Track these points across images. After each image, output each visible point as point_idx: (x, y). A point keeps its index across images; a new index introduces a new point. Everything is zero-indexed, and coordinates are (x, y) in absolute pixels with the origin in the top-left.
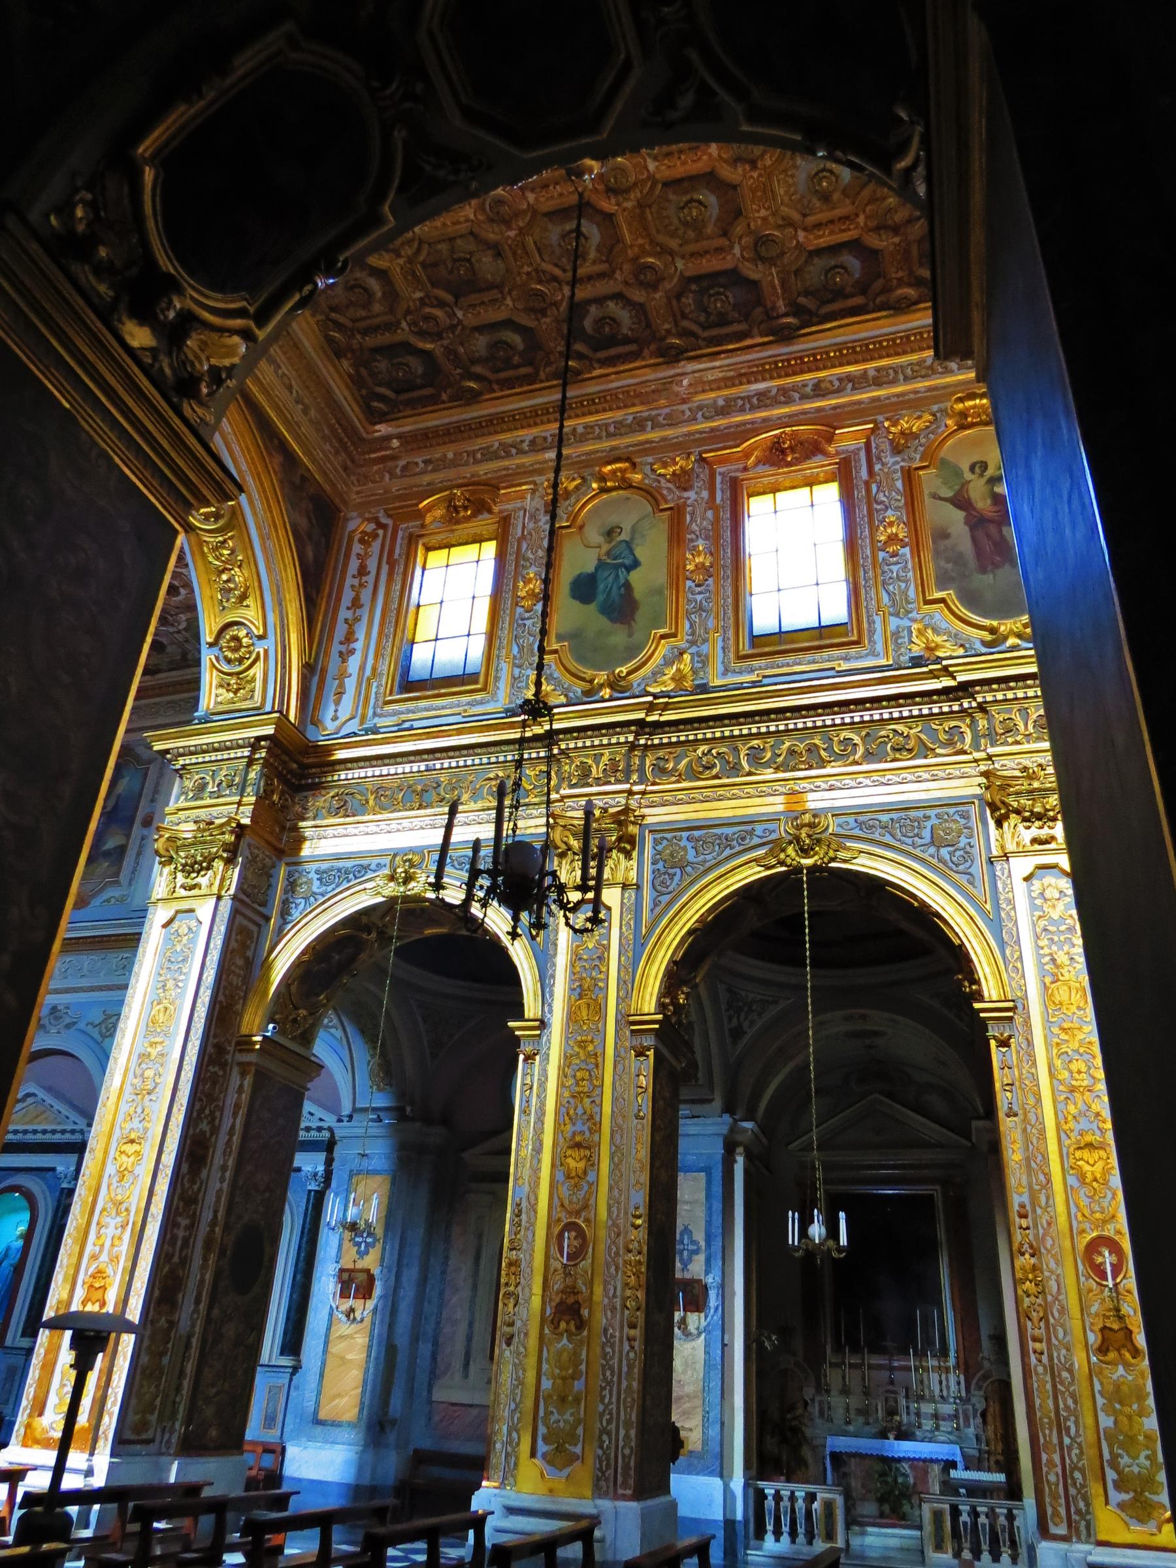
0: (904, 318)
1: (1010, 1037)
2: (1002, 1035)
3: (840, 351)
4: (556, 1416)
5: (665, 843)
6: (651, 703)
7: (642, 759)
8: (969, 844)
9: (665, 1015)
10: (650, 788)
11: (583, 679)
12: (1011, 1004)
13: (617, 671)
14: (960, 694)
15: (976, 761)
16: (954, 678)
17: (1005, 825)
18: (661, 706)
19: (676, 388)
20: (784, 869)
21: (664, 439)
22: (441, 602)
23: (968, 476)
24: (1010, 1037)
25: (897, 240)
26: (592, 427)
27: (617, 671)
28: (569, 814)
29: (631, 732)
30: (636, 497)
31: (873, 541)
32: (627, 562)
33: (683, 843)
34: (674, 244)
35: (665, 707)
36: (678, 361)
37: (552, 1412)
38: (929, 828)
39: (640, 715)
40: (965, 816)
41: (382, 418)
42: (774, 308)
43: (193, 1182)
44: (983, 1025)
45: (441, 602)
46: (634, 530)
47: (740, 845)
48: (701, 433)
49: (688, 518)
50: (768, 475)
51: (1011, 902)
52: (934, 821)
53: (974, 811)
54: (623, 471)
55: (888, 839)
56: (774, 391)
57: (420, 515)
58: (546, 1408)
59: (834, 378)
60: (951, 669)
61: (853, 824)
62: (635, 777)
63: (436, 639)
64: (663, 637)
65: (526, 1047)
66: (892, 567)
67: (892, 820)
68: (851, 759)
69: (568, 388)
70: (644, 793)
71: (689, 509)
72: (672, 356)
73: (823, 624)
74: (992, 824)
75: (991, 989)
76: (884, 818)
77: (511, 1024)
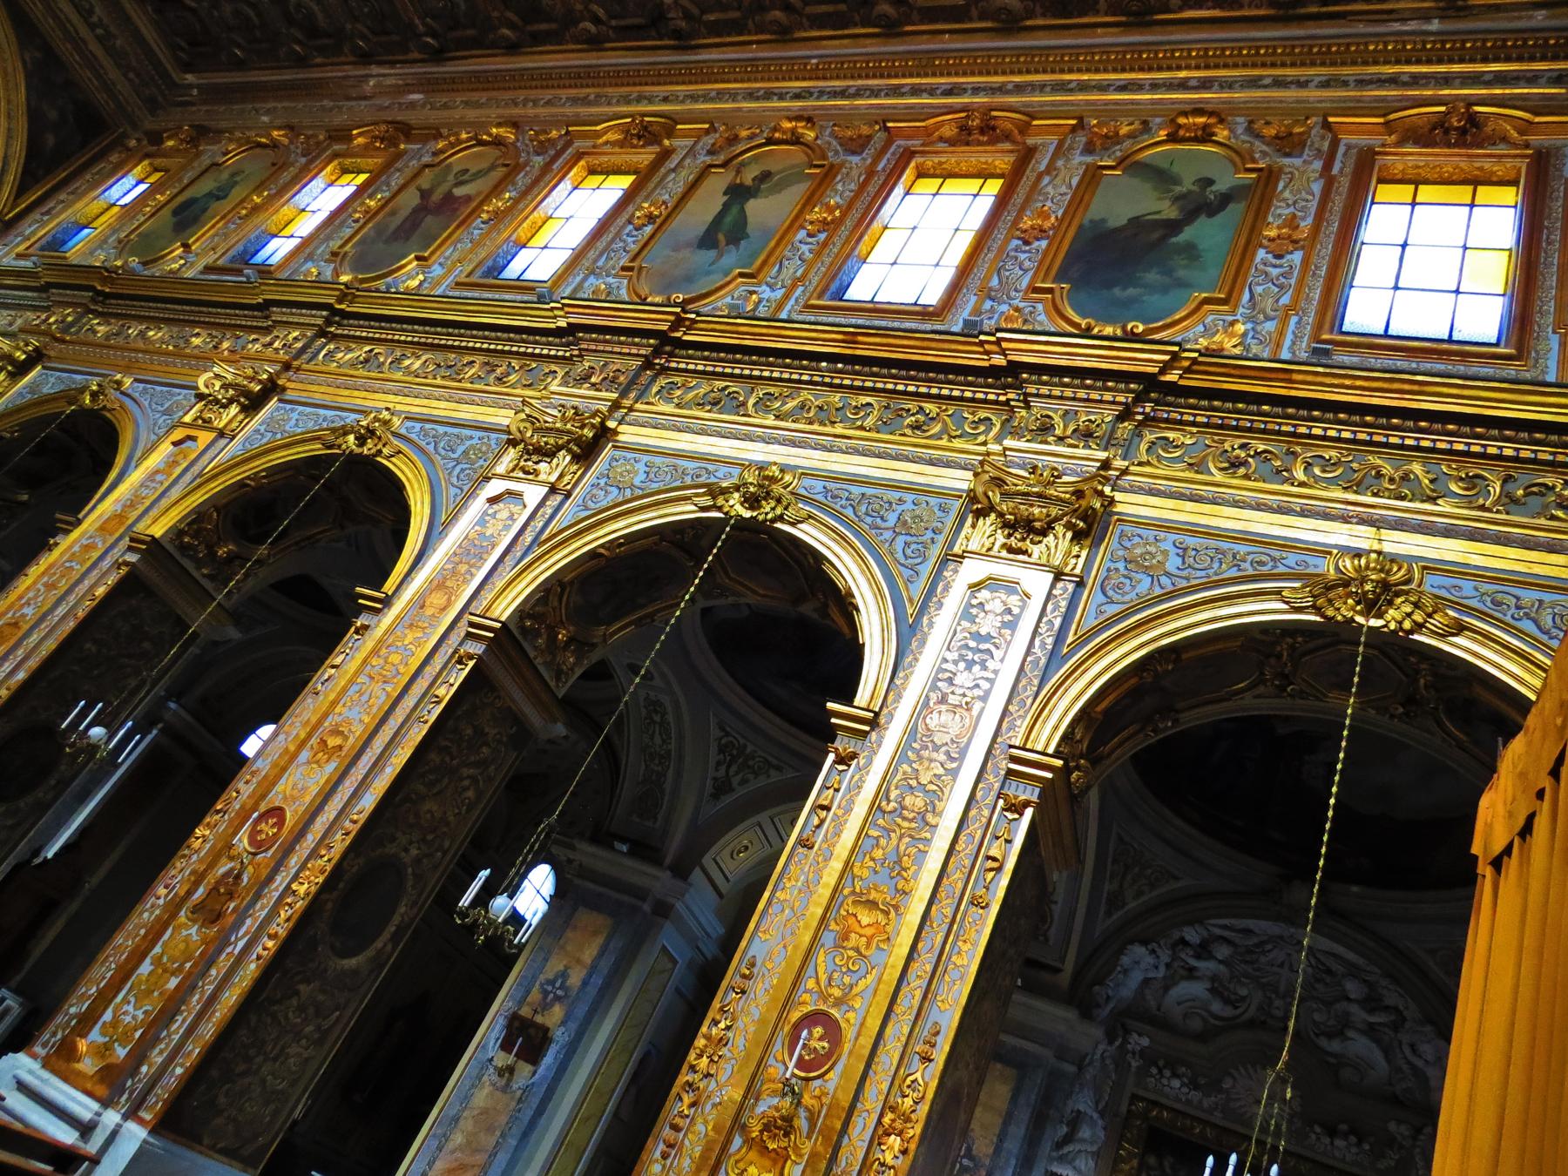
0: (513, 59)
7: (653, 379)
8: (933, 539)
13: (1129, 327)
18: (687, 323)
22: (915, 228)
30: (268, 151)
31: (1015, 222)
36: (370, 64)
40: (943, 509)
41: (188, 67)
45: (915, 228)
49: (839, 178)
50: (1413, 157)
55: (1527, 626)
60: (1004, 345)
63: (1457, 292)
65: (842, 744)
67: (1541, 602)
68: (859, 423)
71: (844, 170)
72: (365, 58)
77: (830, 705)
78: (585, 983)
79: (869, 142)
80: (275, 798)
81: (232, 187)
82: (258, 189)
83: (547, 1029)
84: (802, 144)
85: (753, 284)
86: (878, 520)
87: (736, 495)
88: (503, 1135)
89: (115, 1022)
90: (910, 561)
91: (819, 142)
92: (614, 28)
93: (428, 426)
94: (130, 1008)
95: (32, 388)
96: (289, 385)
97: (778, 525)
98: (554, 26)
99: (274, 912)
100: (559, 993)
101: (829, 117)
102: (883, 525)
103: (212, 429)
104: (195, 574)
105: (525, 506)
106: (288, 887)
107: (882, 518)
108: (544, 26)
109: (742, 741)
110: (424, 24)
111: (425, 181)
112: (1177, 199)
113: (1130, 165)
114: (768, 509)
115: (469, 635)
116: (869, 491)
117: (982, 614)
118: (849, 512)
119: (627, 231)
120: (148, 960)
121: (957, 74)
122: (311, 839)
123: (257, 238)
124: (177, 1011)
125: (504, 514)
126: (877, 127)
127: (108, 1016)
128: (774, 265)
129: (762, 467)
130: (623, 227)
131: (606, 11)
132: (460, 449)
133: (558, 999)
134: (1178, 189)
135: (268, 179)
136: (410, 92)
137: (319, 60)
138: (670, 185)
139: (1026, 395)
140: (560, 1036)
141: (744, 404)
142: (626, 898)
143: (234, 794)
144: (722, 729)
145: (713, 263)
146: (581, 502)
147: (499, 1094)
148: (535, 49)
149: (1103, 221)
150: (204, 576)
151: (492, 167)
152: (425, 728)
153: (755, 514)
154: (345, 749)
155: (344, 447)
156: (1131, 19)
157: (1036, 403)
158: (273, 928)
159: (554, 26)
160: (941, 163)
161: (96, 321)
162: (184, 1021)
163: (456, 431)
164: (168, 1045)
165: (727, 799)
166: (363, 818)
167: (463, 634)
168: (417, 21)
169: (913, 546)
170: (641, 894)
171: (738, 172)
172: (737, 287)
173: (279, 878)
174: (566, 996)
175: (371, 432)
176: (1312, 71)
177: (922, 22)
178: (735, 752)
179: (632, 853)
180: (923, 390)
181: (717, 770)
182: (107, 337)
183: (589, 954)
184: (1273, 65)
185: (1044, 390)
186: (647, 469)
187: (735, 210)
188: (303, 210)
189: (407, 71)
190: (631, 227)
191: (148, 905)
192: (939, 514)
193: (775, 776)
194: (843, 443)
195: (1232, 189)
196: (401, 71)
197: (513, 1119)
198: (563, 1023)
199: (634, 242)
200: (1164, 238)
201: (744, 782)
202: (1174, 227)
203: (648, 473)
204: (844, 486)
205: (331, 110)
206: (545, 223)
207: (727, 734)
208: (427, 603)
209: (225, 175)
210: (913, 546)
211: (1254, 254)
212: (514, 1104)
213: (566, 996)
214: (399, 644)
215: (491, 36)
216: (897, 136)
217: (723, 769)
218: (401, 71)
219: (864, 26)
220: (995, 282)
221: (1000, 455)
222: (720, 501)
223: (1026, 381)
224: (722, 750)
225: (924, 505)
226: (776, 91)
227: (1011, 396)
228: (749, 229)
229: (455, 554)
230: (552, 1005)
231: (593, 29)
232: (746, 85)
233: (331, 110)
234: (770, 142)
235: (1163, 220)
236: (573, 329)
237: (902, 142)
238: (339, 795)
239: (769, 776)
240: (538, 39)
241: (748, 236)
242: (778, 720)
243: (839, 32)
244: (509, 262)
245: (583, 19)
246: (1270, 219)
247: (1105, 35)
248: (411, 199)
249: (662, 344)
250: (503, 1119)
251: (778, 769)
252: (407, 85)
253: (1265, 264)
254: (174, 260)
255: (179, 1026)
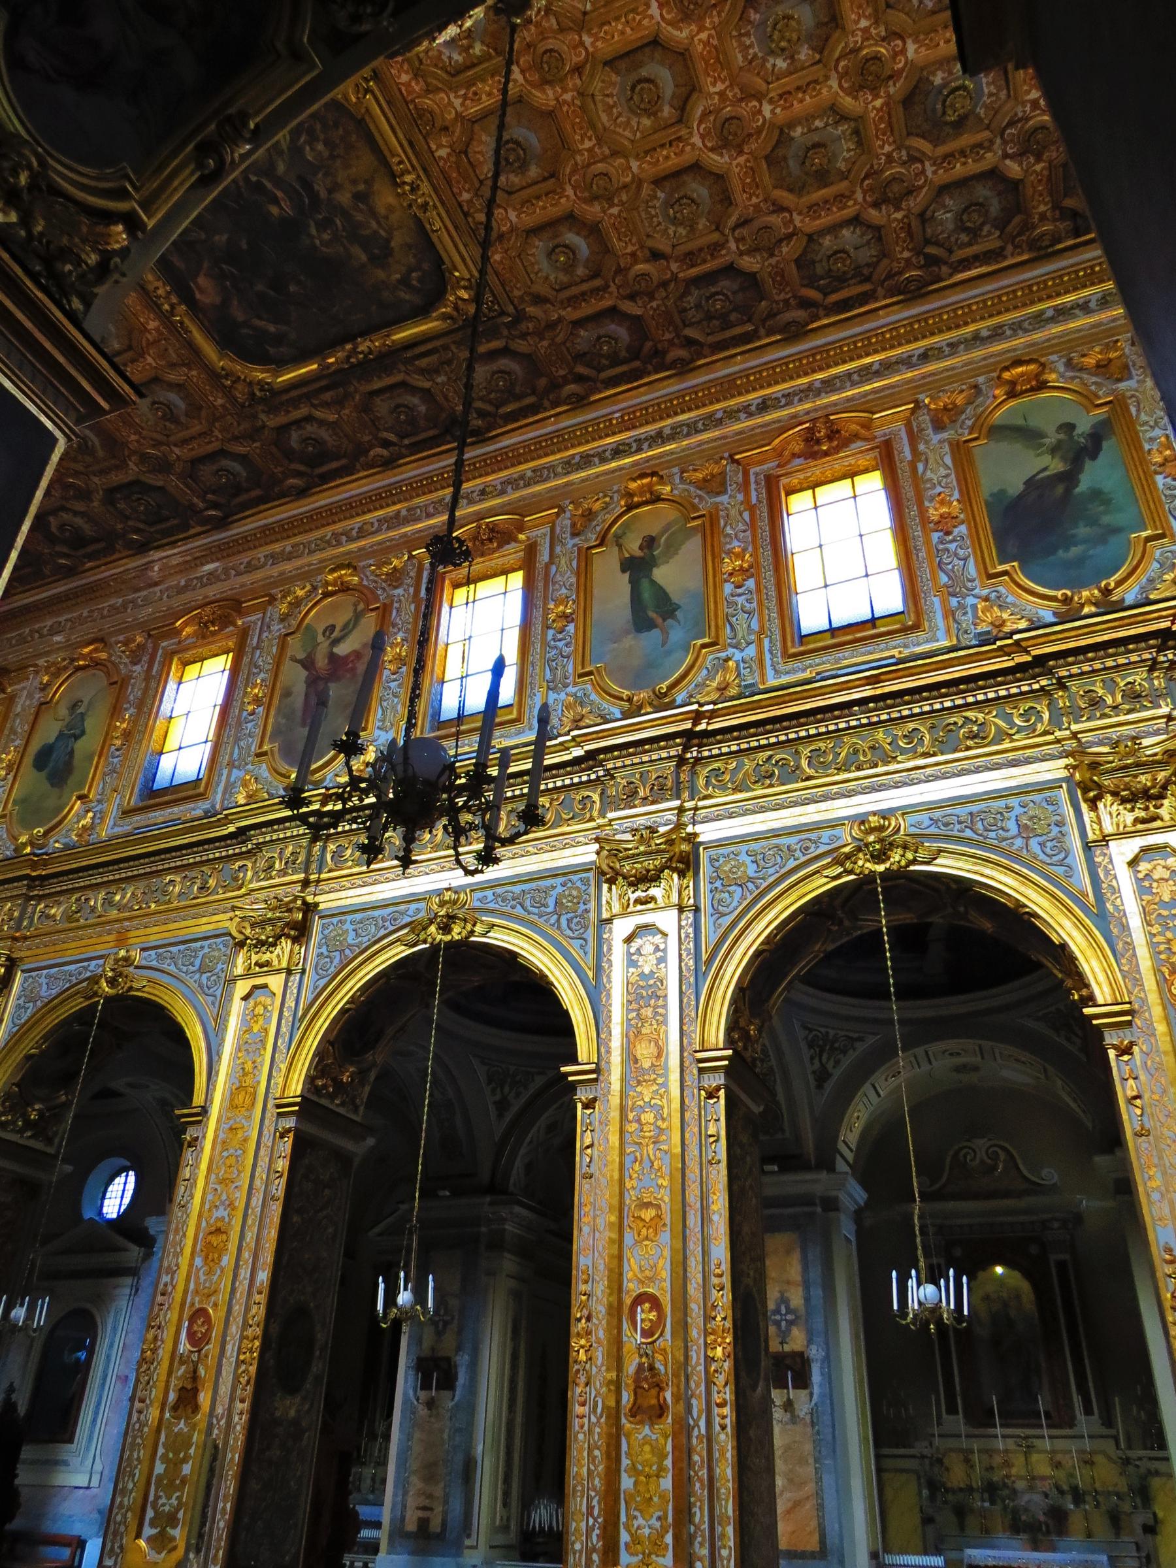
1: (1132, 1044)
2: (1122, 1042)
3: (264, 532)
4: (163, 1500)
5: (331, 927)
6: (697, 711)
7: (694, 773)
9: (735, 1051)
10: (701, 804)
11: (621, 699)
12: (1126, 1007)
14: (591, 763)
15: (1058, 741)
16: (1028, 653)
17: (1100, 805)
18: (708, 714)
19: (150, 574)
20: (852, 877)
21: (361, 549)
22: (821, 546)
23: (320, 638)
24: (1132, 1044)
25: (257, 444)
26: (541, 470)
27: (1103, 584)
28: (617, 837)
29: (525, 782)
32: (77, 732)
33: (348, 926)
34: (79, 467)
35: (713, 714)
37: (635, 1517)
38: (1014, 819)
39: (688, 725)
42: (192, 506)
43: (210, 1272)
44: (1098, 1032)
45: (821, 546)
46: (90, 703)
47: (804, 855)
48: (391, 540)
49: (722, 522)
51: (1116, 891)
52: (1018, 810)
53: (1063, 794)
54: (650, 485)
55: (519, 911)
56: (577, 458)
57: (178, 632)
58: (156, 1491)
59: (374, 520)
60: (1024, 644)
61: (491, 897)
62: (686, 795)
64: (704, 646)
66: (948, 546)
67: (971, 814)
69: (466, 449)
70: (696, 809)
72: (143, 548)
73: (834, 625)
74: (1084, 807)
75: (1102, 992)
76: (517, 889)
77: (563, 1069)
78: (807, 1299)
79: (725, 478)
80: (632, 1288)
81: (83, 720)
82: (116, 711)
83: (801, 1354)
84: (664, 500)
85: (719, 651)
86: (1001, 832)
87: (861, 855)
88: (816, 1461)
89: (636, 1539)
90: (1055, 858)
91: (676, 492)
92: (407, 447)
93: (499, 890)
94: (641, 1521)
95: (28, 996)
96: (318, 899)
97: (912, 868)
98: (344, 462)
99: (709, 1383)
100: (789, 1317)
101: (669, 465)
102: (548, 910)
103: (278, 971)
104: (331, 1107)
105: (665, 935)
106: (706, 1356)
107: (1002, 829)
108: (335, 465)
109: (823, 1030)
110: (204, 500)
111: (296, 647)
112: (1054, 450)
113: (998, 432)
114: (897, 858)
115: (701, 1071)
116: (975, 808)
117: (1155, 885)
118: (968, 833)
119: (550, 637)
120: (624, 1475)
121: (762, 387)
122: (695, 1308)
123: (150, 763)
124: (690, 1506)
125: (648, 949)
126: (724, 462)
127: (624, 1537)
128: (725, 626)
129: (862, 820)
130: (544, 635)
131: (397, 435)
132: (551, 902)
133: (791, 1323)
134: (1047, 441)
135: (117, 701)
136: (203, 564)
137: (89, 565)
138: (558, 578)
139: (1059, 679)
140: (815, 1353)
141: (798, 767)
142: (798, 1210)
143: (584, 1298)
144: (806, 1028)
145: (664, 644)
146: (711, 910)
147: (789, 1427)
148: (325, 487)
149: (1002, 492)
150: (337, 1105)
151: (358, 616)
152: (723, 1167)
153: (888, 865)
154: (667, 1219)
155: (429, 940)
156: (909, 296)
157: (1073, 685)
158: (717, 1398)
159: (344, 462)
160: (806, 478)
161: (42, 906)
162: (701, 1509)
163: (533, 885)
164: (703, 1536)
165: (829, 1086)
166: (726, 1267)
167: (695, 1071)
168: (195, 500)
169: (1049, 844)
170: (807, 1200)
171: (620, 546)
172: (705, 658)
173: (693, 1354)
174: (797, 1317)
175: (452, 918)
176: (1085, 293)
177: (713, 354)
178: (821, 1042)
179: (783, 1170)
180: (959, 702)
181: (812, 1064)
182: (69, 917)
183: (794, 1270)
184: (1050, 297)
185: (1075, 670)
186: (753, 858)
187: (645, 584)
188: (171, 717)
189: (189, 546)
190: (551, 633)
191: (577, 1428)
192: (1051, 808)
193: (861, 1047)
194: (918, 774)
195: (1094, 426)
196: (183, 548)
197: (817, 1443)
198: (810, 1341)
199: (566, 645)
200: (1068, 491)
201: (837, 1063)
202: (1069, 478)
203: (755, 862)
204: (949, 812)
205: (124, 606)
206: (446, 651)
207: (811, 1030)
208: (639, 1057)
209: (63, 711)
210: (1049, 844)
211: (1155, 483)
212: (809, 1429)
213: (797, 1317)
214: (641, 1103)
215: (276, 490)
216: (748, 465)
217: (816, 1061)
218: (183, 548)
219: (657, 372)
220: (944, 579)
221: (1069, 739)
222: (848, 865)
223: (1054, 667)
224: (811, 1046)
225: (1032, 805)
226: (592, 452)
227: (1043, 683)
228: (675, 598)
229: (630, 1002)
230: (789, 1330)
231: (385, 452)
232: (558, 456)
233: (124, 606)
234: (630, 507)
235: (1055, 475)
236: (591, 755)
237: (758, 469)
238: (693, 1259)
239: (854, 1050)
240: (325, 478)
241: (679, 607)
242: (840, 998)
243: (636, 384)
244: (441, 701)
245: (372, 447)
246: (1147, 447)
247: (888, 315)
248: (295, 676)
249: (689, 740)
250: (808, 1447)
251: (861, 1039)
252: (196, 559)
253: (1169, 488)
254: (79, 817)
255: (700, 1515)
